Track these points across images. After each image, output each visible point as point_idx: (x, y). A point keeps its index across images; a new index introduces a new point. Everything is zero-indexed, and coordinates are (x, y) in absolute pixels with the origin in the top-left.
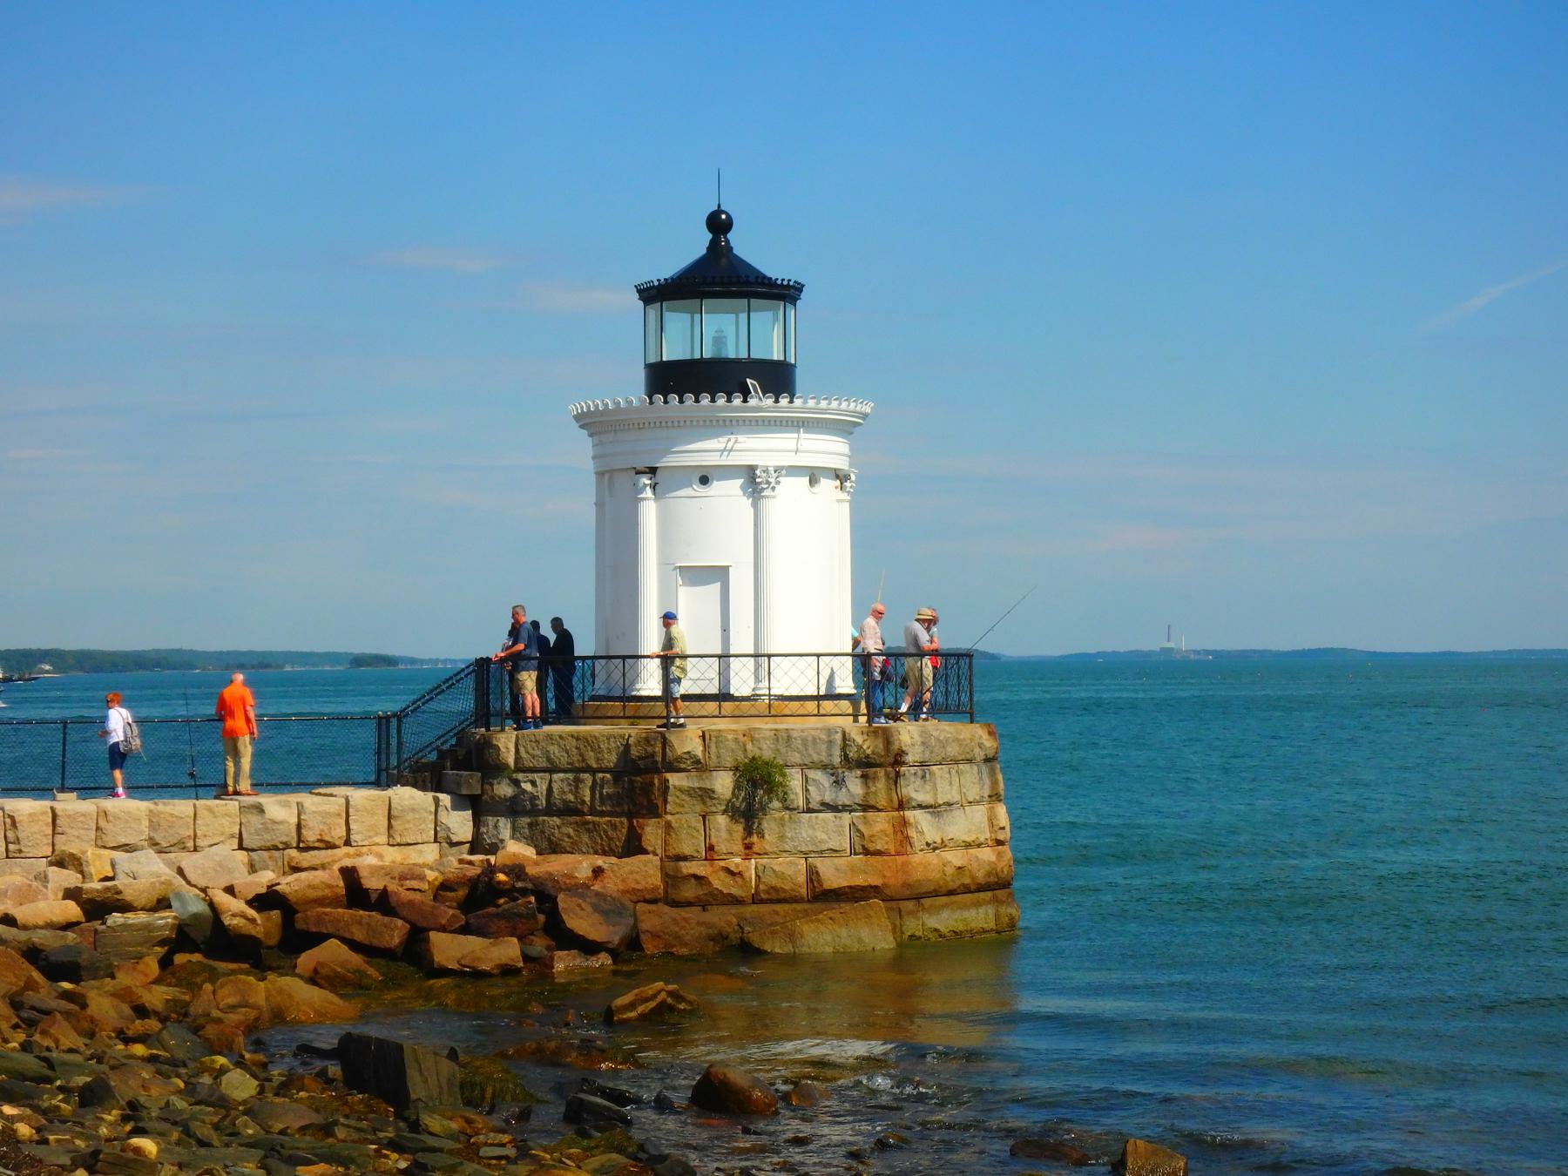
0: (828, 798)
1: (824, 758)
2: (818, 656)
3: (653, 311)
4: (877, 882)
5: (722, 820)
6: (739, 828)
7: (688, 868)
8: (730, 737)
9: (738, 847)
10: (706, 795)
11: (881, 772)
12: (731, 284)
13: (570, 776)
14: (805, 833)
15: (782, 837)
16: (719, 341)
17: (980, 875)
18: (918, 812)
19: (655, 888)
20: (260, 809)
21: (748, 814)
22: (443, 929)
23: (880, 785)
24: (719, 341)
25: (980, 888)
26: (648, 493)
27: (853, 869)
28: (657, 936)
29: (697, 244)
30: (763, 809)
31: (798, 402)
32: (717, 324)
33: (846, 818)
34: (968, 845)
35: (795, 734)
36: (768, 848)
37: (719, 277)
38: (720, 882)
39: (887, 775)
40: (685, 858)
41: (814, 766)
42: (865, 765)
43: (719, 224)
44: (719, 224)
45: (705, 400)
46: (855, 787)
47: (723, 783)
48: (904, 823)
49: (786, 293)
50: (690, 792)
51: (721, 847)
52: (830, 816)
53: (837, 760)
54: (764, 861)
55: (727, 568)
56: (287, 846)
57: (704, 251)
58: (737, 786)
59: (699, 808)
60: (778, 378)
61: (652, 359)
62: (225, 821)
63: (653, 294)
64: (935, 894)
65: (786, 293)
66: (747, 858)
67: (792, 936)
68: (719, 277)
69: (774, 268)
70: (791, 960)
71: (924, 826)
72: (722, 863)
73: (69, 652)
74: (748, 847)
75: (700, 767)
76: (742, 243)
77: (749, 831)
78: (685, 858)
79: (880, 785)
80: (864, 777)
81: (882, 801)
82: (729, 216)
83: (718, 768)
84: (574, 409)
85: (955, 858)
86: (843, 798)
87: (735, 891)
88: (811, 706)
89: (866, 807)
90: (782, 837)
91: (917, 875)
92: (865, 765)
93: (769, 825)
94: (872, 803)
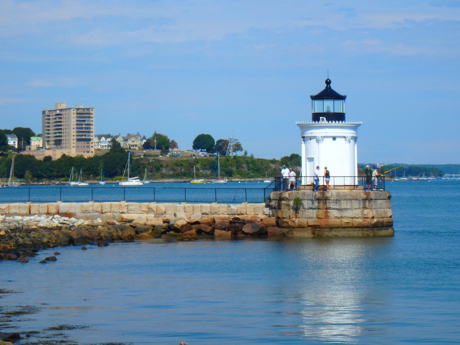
0: (311, 206)
1: (311, 198)
4: (319, 224)
5: (292, 210)
6: (294, 212)
7: (285, 220)
9: (294, 216)
10: (288, 205)
11: (322, 201)
14: (307, 213)
15: (302, 214)
16: (328, 108)
17: (356, 225)
18: (333, 210)
19: (274, 224)
20: (230, 206)
21: (296, 209)
22: (218, 229)
23: (321, 204)
24: (328, 108)
25: (356, 227)
26: (303, 142)
27: (315, 221)
28: (270, 233)
29: (323, 87)
30: (299, 208)
31: (346, 123)
32: (329, 105)
33: (315, 211)
34: (352, 218)
36: (300, 216)
37: (328, 94)
38: (290, 223)
39: (323, 202)
40: (285, 218)
42: (318, 200)
43: (328, 82)
44: (328, 82)
45: (334, 122)
46: (316, 204)
47: (291, 203)
48: (327, 212)
49: (342, 98)
50: (286, 204)
51: (291, 216)
52: (311, 210)
53: (314, 199)
54: (299, 219)
55: (313, 158)
56: (235, 214)
58: (294, 204)
59: (288, 208)
60: (340, 117)
61: (313, 112)
62: (224, 209)
63: (314, 98)
64: (334, 228)
65: (342, 98)
66: (296, 218)
67: (292, 234)
68: (328, 94)
69: (341, 93)
70: (292, 238)
71: (334, 213)
74: (296, 216)
75: (288, 200)
76: (333, 87)
77: (296, 213)
78: (285, 218)
79: (321, 204)
80: (318, 202)
81: (321, 207)
82: (330, 80)
83: (291, 200)
84: (297, 123)
85: (345, 220)
86: (314, 207)
87: (293, 225)
88: (343, 187)
89: (319, 209)
90: (302, 214)
91: (330, 223)
92: (318, 200)
93: (300, 212)
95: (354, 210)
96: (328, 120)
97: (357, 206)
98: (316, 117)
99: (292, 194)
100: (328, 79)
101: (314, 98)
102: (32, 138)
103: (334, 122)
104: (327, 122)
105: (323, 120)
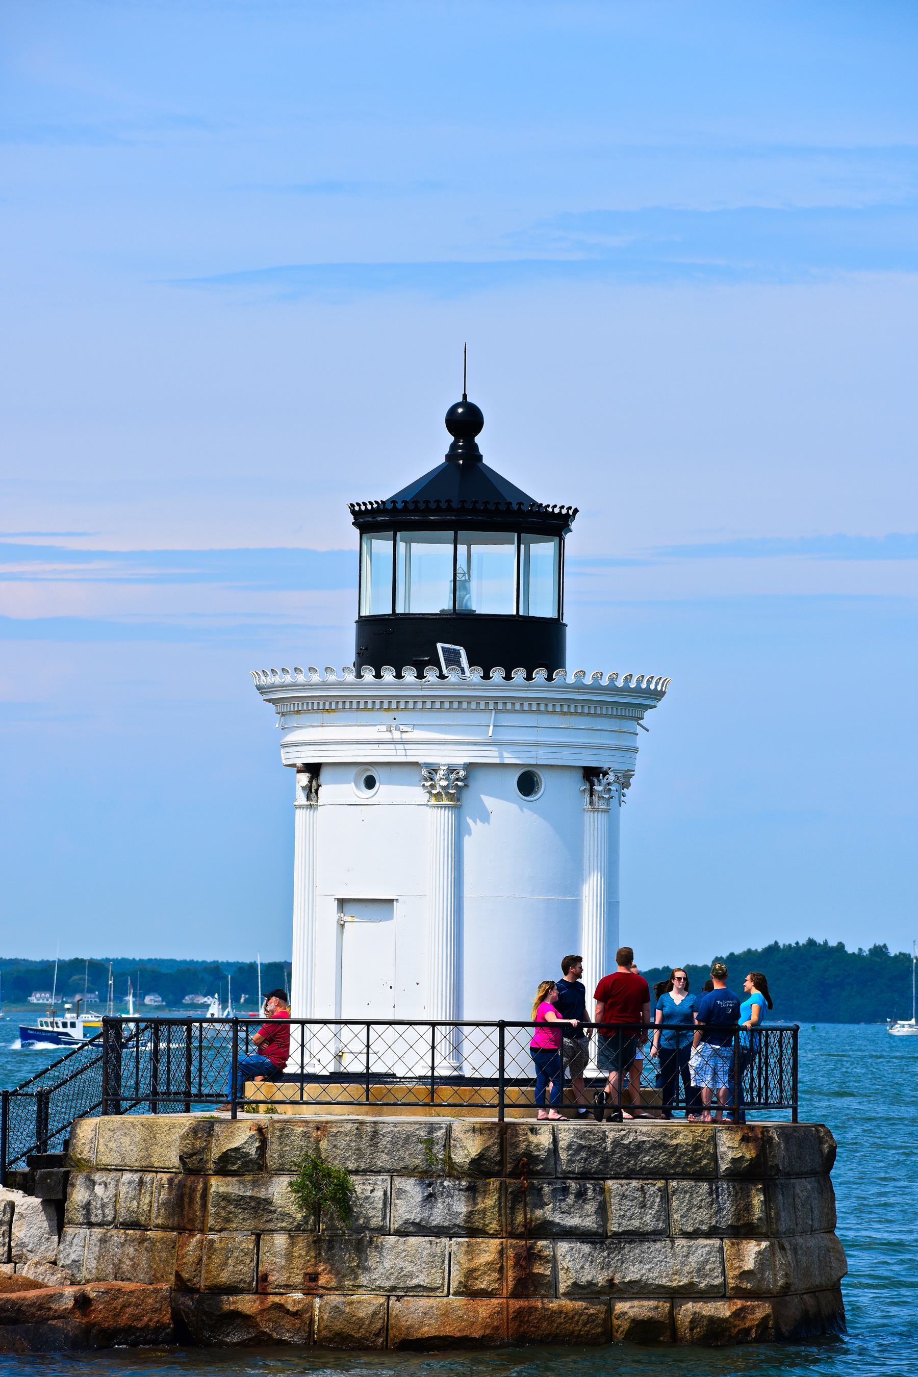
2: (368, 1024)
3: (382, 546)
5: (281, 1241)
8: (299, 1130)
12: (428, 511)
13: (136, 1177)
29: (434, 449)
35: (384, 1130)
37: (467, 498)
39: (502, 1189)
41: (406, 1172)
43: (465, 422)
44: (465, 422)
50: (239, 1201)
57: (442, 460)
63: (372, 520)
65: (553, 524)
68: (467, 498)
69: (544, 493)
72: (277, 1299)
73: (228, 964)
83: (281, 1171)
94: (479, 1224)
95: (681, 1242)
96: (483, 660)
97: (703, 1218)
98: (392, 642)
99: (117, 1010)
100: (465, 403)
101: (372, 520)
102: (453, 532)
103: (497, 674)
104: (474, 675)
105: (453, 659)
